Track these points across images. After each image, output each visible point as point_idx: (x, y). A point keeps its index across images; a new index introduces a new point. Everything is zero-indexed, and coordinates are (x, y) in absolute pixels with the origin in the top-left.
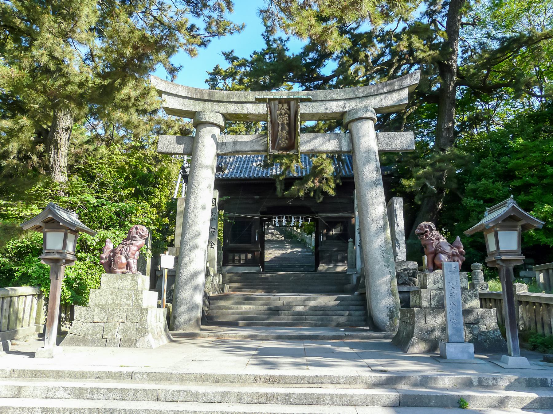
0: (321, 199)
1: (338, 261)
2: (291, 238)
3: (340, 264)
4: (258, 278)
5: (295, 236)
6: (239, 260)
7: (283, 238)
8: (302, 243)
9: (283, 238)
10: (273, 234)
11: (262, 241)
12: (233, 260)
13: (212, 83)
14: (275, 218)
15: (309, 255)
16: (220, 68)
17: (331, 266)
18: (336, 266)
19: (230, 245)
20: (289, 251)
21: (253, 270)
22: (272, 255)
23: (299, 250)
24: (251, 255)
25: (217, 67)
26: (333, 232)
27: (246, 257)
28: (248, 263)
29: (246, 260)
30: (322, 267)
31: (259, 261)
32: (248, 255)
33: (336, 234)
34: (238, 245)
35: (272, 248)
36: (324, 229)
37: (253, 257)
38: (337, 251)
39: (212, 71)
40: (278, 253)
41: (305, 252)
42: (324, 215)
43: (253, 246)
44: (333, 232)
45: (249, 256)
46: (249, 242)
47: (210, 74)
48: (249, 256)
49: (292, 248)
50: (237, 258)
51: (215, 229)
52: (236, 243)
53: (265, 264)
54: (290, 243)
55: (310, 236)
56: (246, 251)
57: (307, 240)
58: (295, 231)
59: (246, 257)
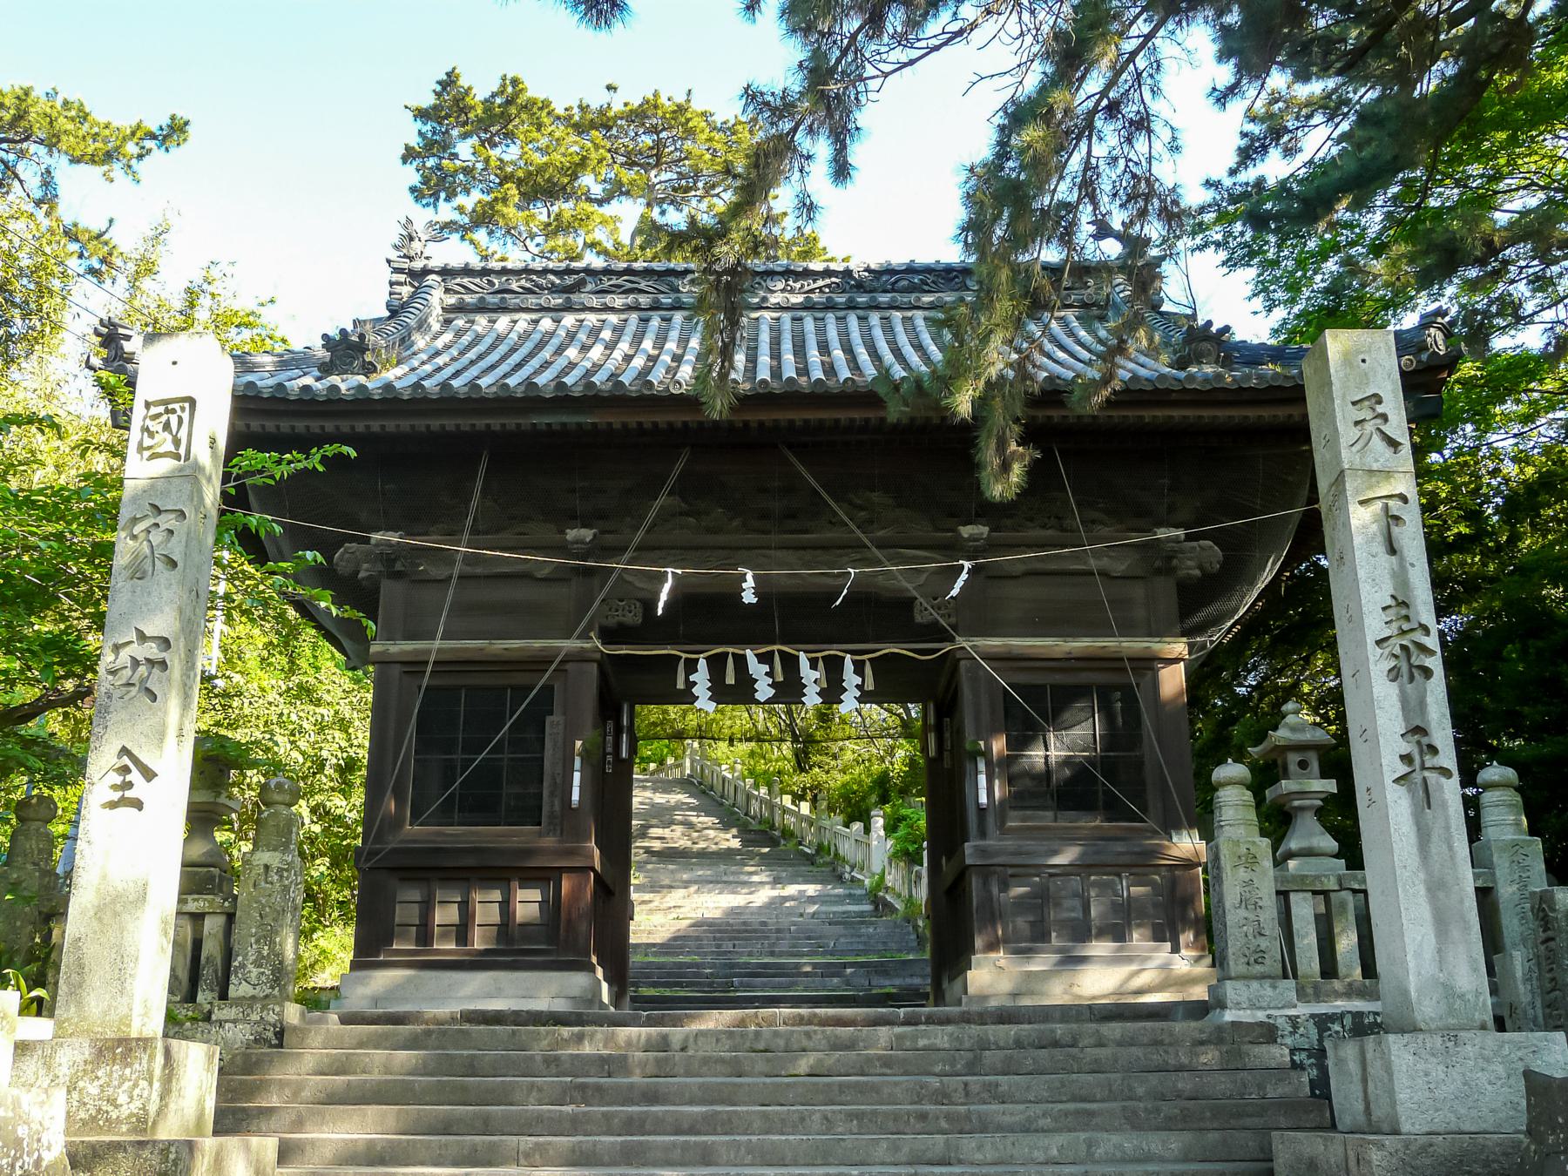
0: (1017, 473)
1: (1082, 932)
2: (773, 843)
3: (1100, 948)
4: (553, 1063)
5: (787, 834)
6: (462, 932)
7: (735, 844)
8: (820, 862)
9: (735, 844)
10: (689, 825)
11: (613, 820)
12: (425, 935)
13: (431, 162)
14: (691, 667)
15: (861, 914)
16: (464, 82)
17: (1041, 963)
18: (1072, 961)
19: (410, 829)
20: (763, 896)
21: (546, 991)
22: (682, 912)
23: (811, 889)
24: (535, 895)
25: (449, 81)
26: (1051, 751)
27: (506, 906)
28: (514, 950)
29: (506, 927)
30: (990, 974)
31: (590, 930)
32: (521, 894)
33: (1067, 762)
34: (458, 833)
35: (686, 884)
36: (994, 731)
37: (552, 907)
38: (1080, 868)
39: (428, 100)
40: (712, 904)
41: (840, 900)
42: (994, 643)
43: (549, 842)
44: (1051, 751)
45: (528, 903)
46: (529, 813)
47: (422, 114)
48: (528, 903)
49: (776, 881)
50: (445, 915)
51: (165, 643)
52: (445, 815)
53: (635, 959)
54: (766, 861)
55: (857, 826)
56: (501, 872)
57: (846, 849)
58: (785, 810)
59: (506, 906)
